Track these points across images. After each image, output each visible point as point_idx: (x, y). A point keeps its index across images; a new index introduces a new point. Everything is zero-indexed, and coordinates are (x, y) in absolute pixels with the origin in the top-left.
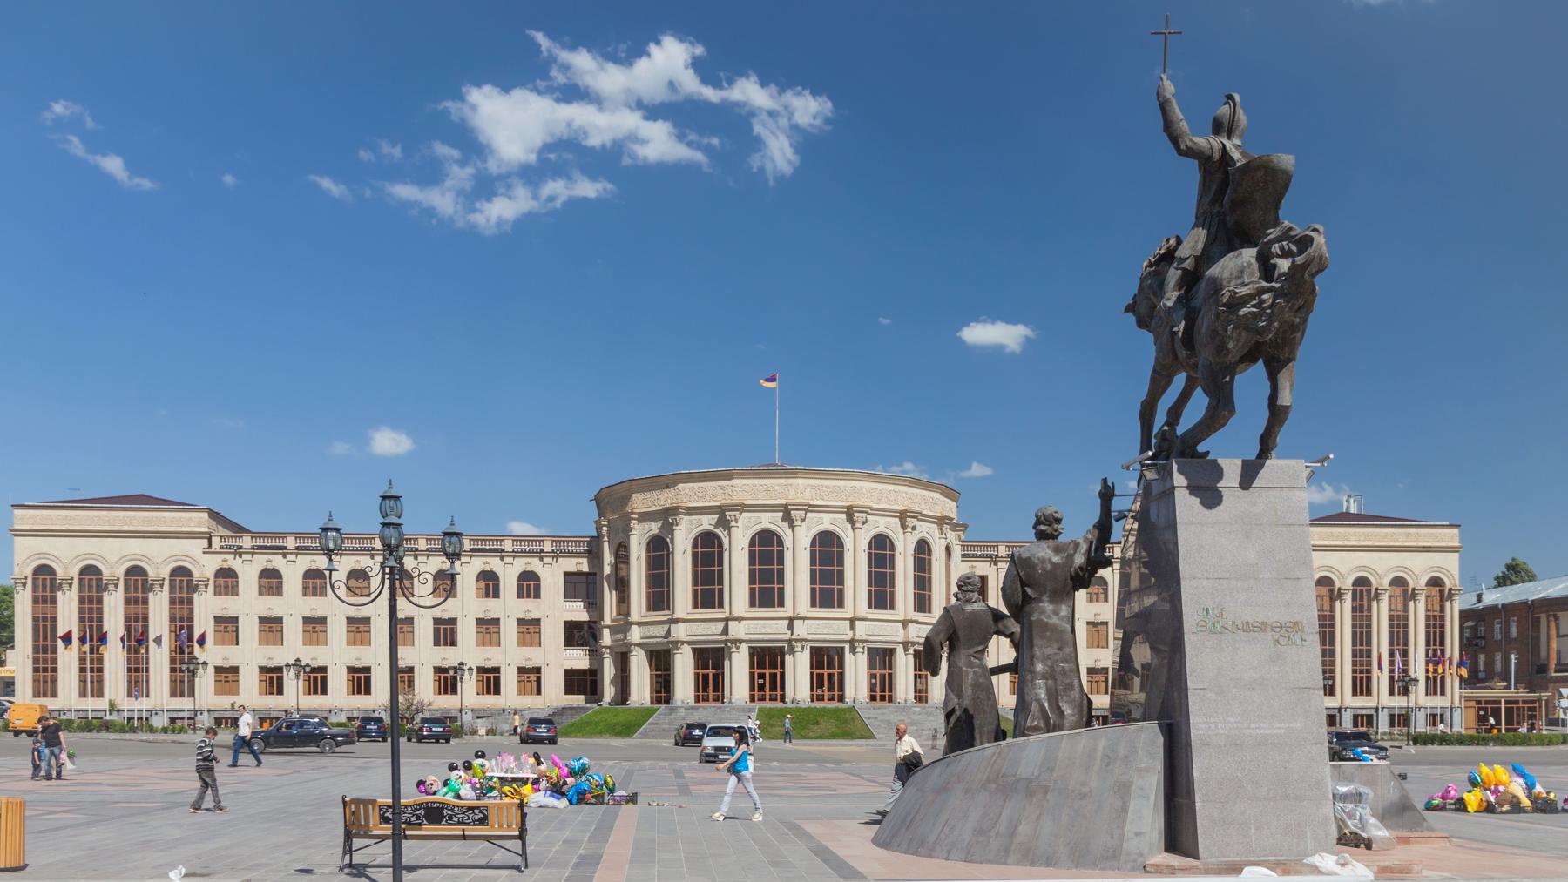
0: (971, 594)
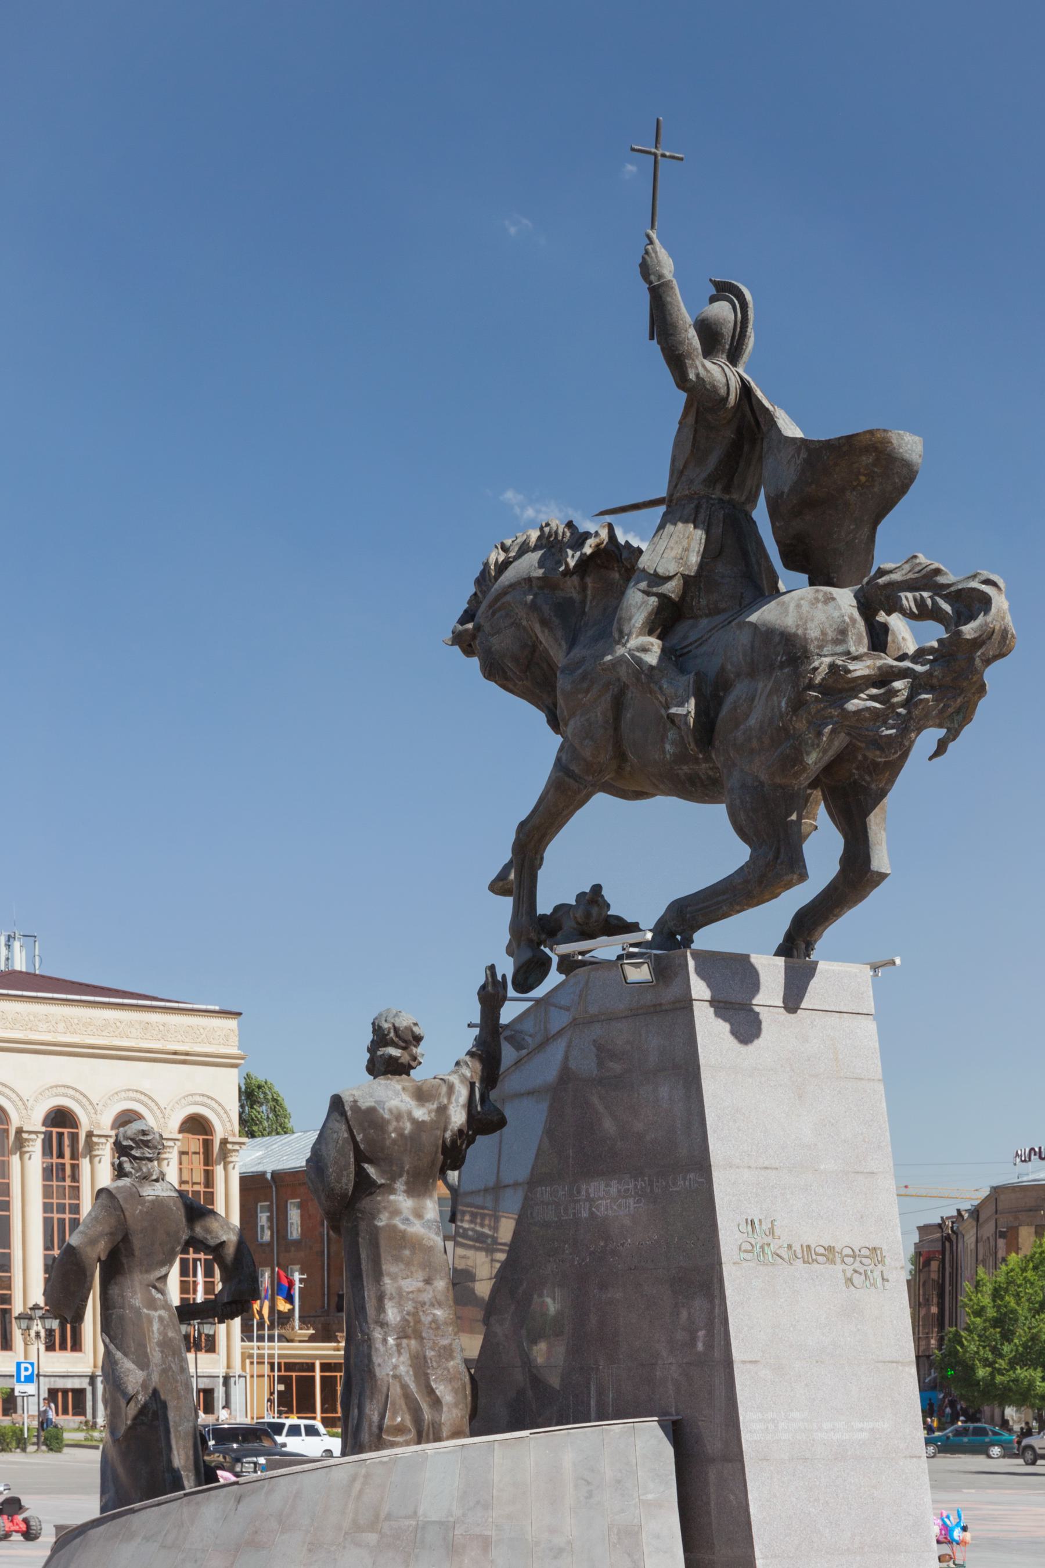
0: (150, 1165)
